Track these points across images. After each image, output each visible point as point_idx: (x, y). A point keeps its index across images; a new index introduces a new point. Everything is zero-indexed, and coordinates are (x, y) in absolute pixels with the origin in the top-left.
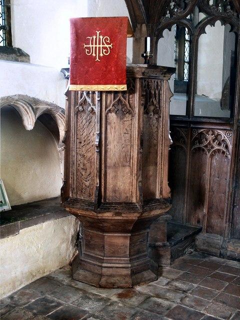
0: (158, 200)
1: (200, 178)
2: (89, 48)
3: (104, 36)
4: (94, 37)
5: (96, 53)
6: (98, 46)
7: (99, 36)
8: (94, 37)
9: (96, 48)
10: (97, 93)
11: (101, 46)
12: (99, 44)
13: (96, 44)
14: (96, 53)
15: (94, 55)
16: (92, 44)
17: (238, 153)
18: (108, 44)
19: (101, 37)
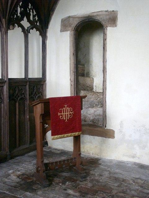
0: (37, 162)
1: (42, 37)
2: (62, 115)
3: (69, 108)
4: (64, 109)
5: (65, 118)
6: (66, 114)
7: (66, 119)
8: (64, 109)
9: (65, 114)
10: (99, 111)
11: (68, 113)
12: (67, 112)
13: (65, 112)
14: (65, 118)
15: (65, 119)
16: (63, 113)
17: (2, 45)
18: (71, 111)
19: (68, 108)
